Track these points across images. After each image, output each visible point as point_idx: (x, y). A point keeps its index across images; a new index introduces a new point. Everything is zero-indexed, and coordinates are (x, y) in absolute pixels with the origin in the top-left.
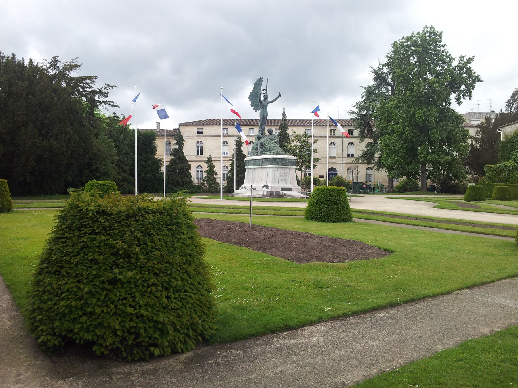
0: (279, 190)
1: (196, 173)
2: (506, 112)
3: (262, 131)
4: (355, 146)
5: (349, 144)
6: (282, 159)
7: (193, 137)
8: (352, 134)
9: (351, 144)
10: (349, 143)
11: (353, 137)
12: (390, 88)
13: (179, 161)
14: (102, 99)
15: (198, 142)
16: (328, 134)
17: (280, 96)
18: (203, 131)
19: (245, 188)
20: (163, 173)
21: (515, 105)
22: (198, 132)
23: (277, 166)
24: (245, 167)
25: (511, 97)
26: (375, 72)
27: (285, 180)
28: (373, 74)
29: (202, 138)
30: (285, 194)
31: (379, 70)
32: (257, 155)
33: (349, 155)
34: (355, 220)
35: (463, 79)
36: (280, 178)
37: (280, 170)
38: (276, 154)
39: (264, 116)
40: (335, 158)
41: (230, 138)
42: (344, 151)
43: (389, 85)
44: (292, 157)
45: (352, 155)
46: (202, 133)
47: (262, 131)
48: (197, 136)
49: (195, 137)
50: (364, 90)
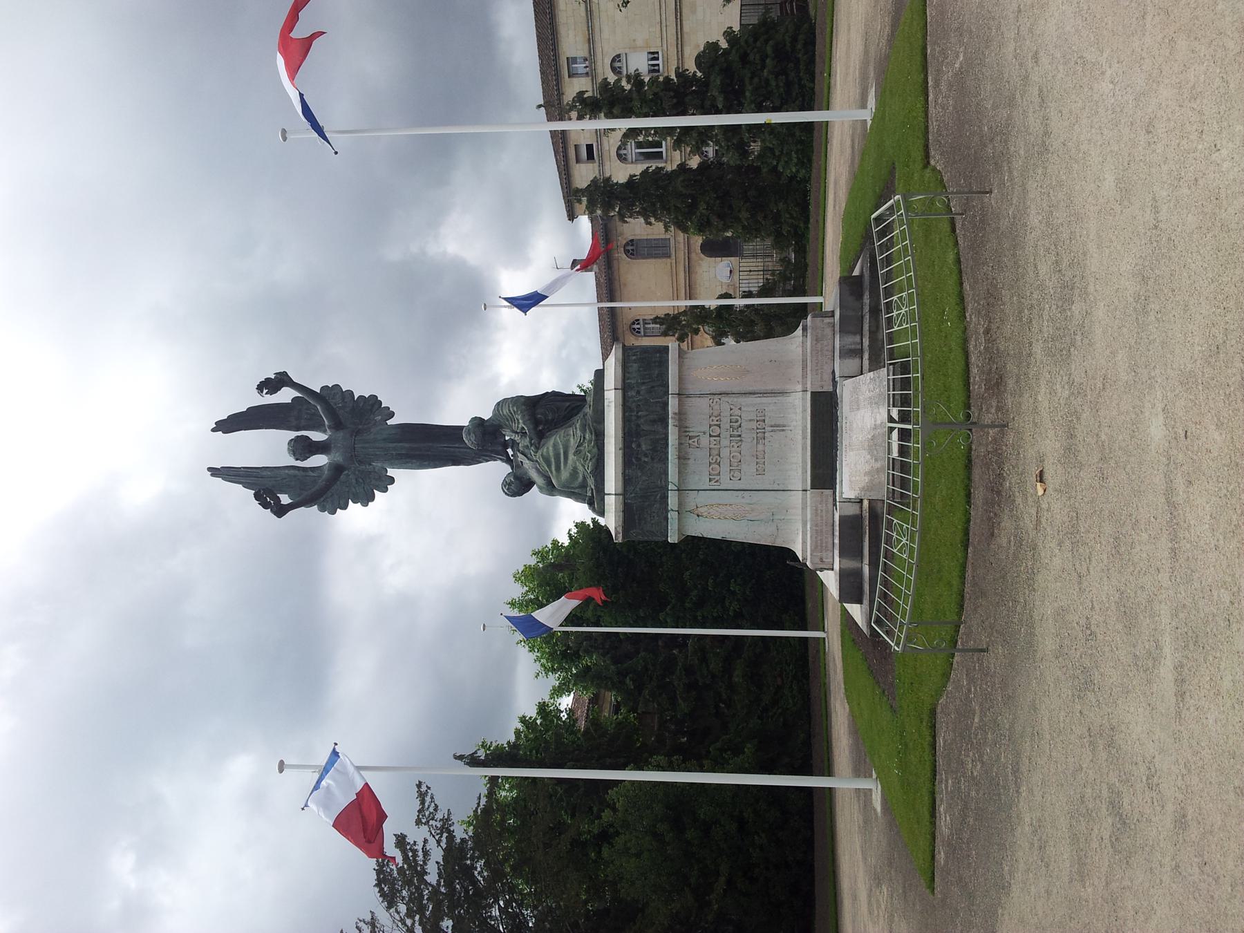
18: (583, 144)
22: (590, 156)
27: (761, 437)
29: (606, 146)
35: (392, 415)
36: (749, 477)
37: (699, 477)
41: (598, 51)
46: (590, 147)
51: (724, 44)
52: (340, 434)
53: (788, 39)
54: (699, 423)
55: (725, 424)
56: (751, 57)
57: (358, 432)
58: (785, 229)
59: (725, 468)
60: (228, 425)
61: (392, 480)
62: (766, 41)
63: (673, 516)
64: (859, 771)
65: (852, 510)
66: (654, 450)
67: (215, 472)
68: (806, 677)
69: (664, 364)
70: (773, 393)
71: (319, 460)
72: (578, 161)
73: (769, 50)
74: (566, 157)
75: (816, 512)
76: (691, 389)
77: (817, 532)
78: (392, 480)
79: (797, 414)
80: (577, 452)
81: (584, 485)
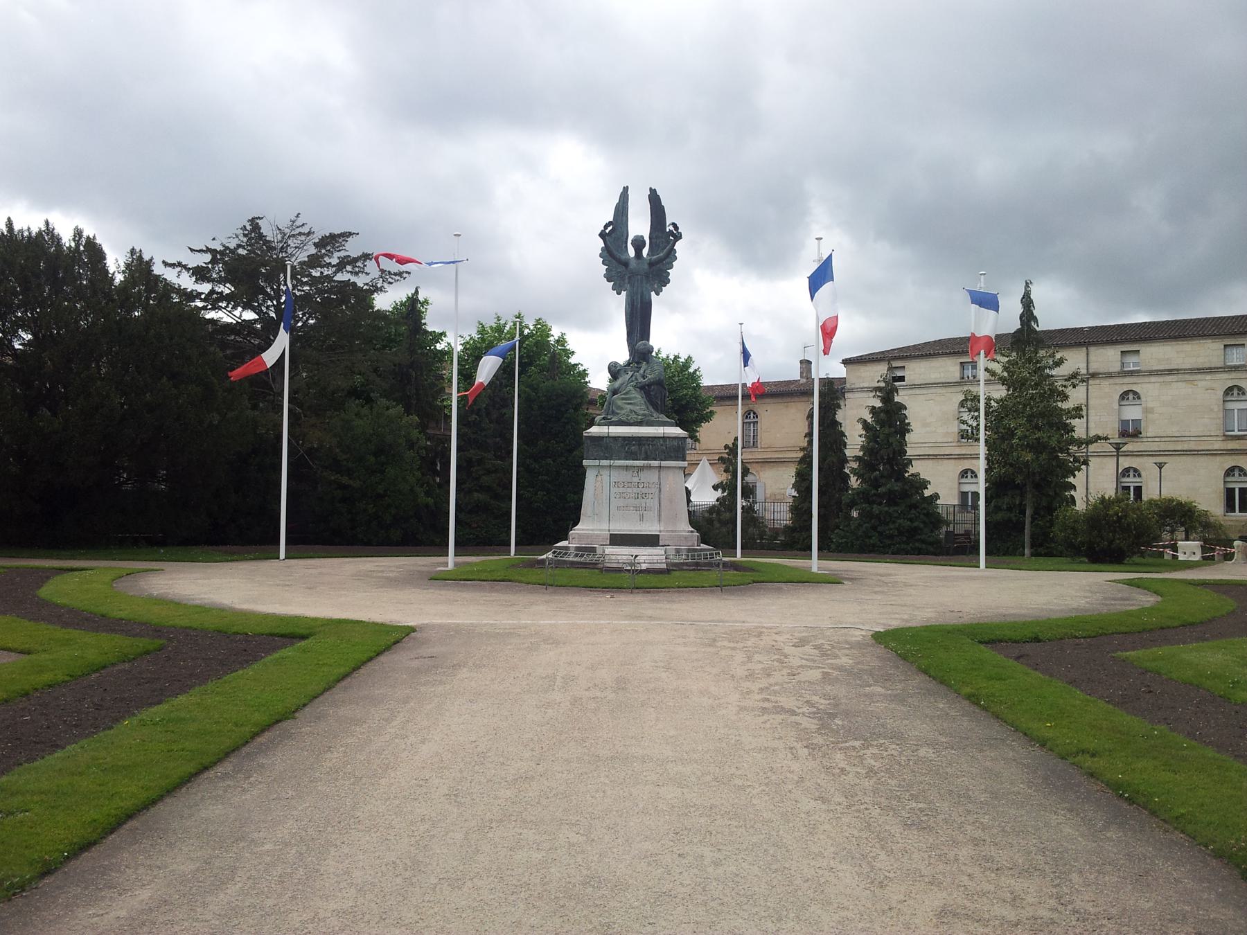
27: (637, 509)
35: (657, 294)
37: (617, 476)
51: (927, 493)
52: (646, 266)
53: (923, 537)
54: (646, 477)
55: (644, 491)
56: (913, 511)
57: (647, 277)
58: (796, 535)
59: (621, 490)
60: (654, 198)
61: (619, 293)
62: (924, 522)
63: (597, 462)
64: (456, 564)
65: (599, 552)
66: (632, 453)
67: (626, 189)
68: (478, 544)
69: (677, 459)
70: (660, 515)
71: (631, 252)
72: (891, 369)
73: (916, 524)
74: (895, 358)
75: (598, 536)
76: (663, 473)
77: (588, 536)
78: (619, 293)
79: (648, 527)
80: (631, 411)
81: (614, 413)
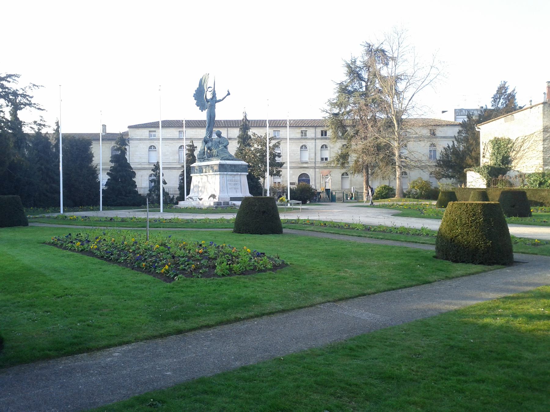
0: (228, 200)
1: (142, 183)
2: (493, 108)
3: (210, 133)
4: (329, 148)
5: (322, 147)
6: (231, 165)
7: (145, 142)
8: (326, 135)
9: (324, 147)
10: (323, 146)
11: (326, 139)
12: (364, 84)
13: (122, 170)
14: (24, 101)
15: (151, 146)
16: (319, 135)
17: (229, 94)
19: (191, 198)
20: (267, 190)
21: (502, 100)
23: (225, 173)
24: (191, 175)
25: (498, 91)
26: (349, 66)
28: (347, 69)
29: (155, 142)
30: (234, 204)
31: (352, 64)
32: (203, 161)
33: (322, 159)
34: (284, 230)
36: (229, 186)
37: (229, 178)
38: (225, 160)
39: (211, 116)
40: (306, 163)
42: (317, 155)
43: (362, 80)
44: (244, 163)
45: (326, 159)
47: (210, 133)
48: (321, 139)
49: (147, 142)
50: (337, 86)
